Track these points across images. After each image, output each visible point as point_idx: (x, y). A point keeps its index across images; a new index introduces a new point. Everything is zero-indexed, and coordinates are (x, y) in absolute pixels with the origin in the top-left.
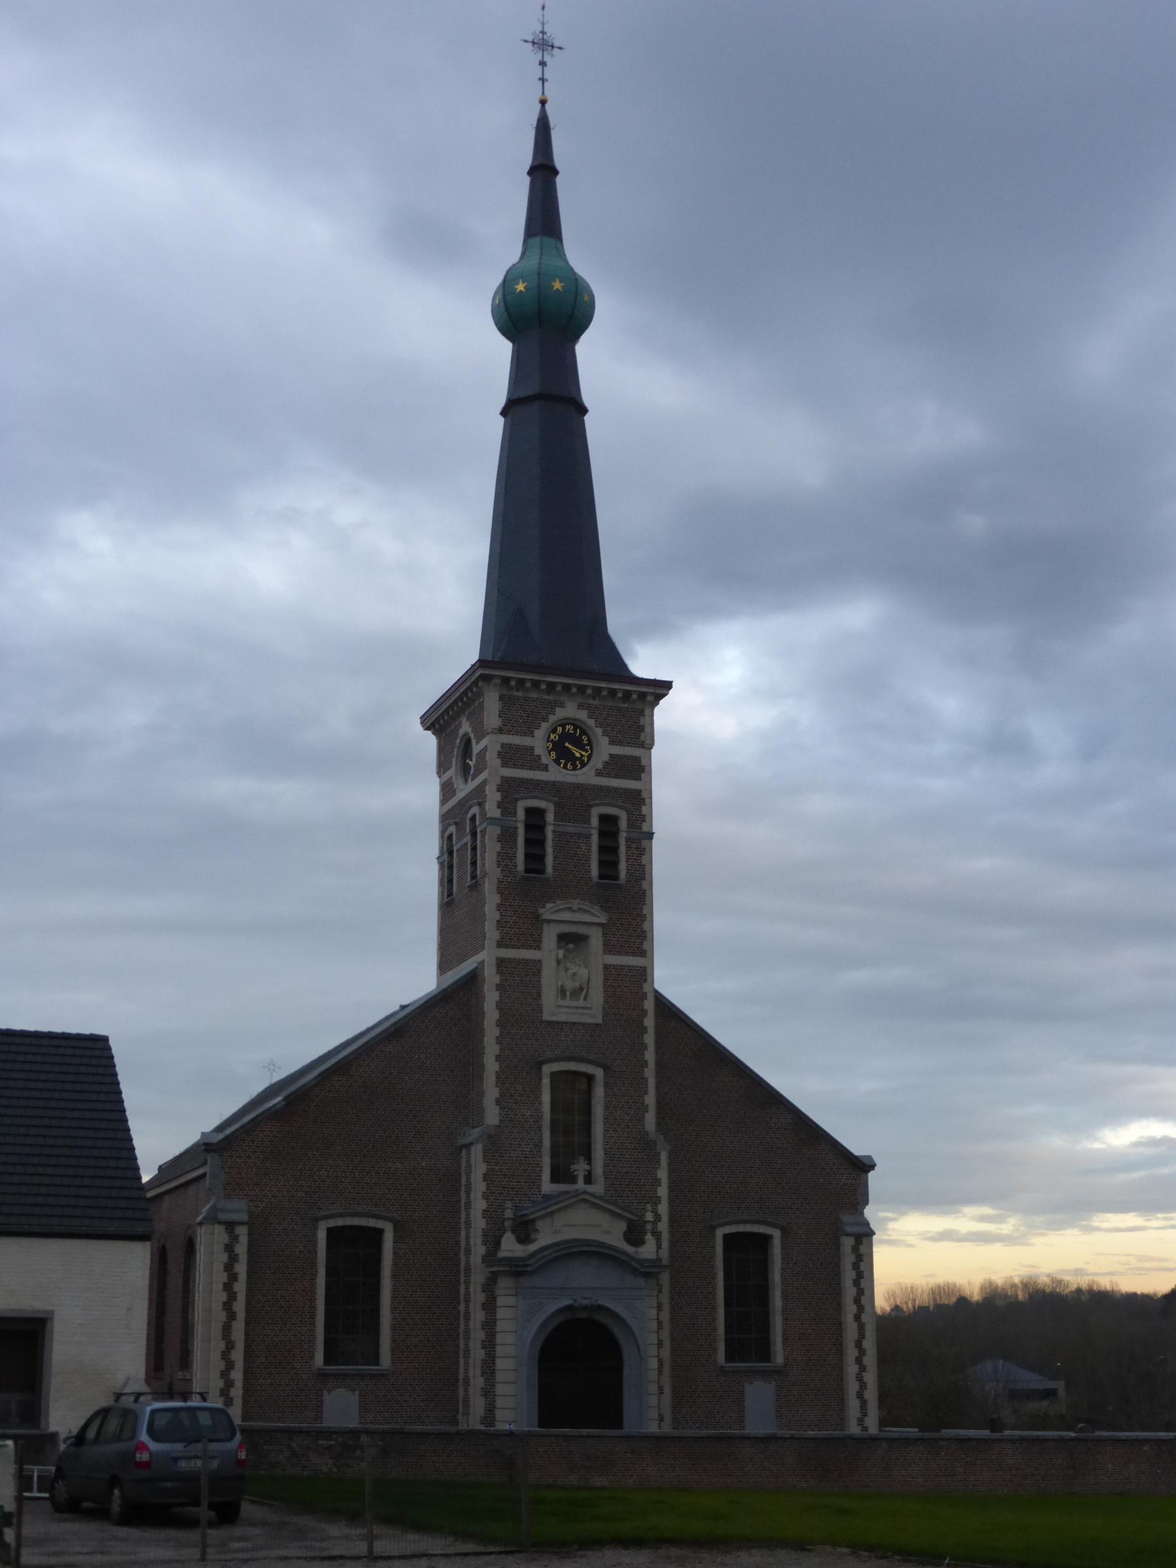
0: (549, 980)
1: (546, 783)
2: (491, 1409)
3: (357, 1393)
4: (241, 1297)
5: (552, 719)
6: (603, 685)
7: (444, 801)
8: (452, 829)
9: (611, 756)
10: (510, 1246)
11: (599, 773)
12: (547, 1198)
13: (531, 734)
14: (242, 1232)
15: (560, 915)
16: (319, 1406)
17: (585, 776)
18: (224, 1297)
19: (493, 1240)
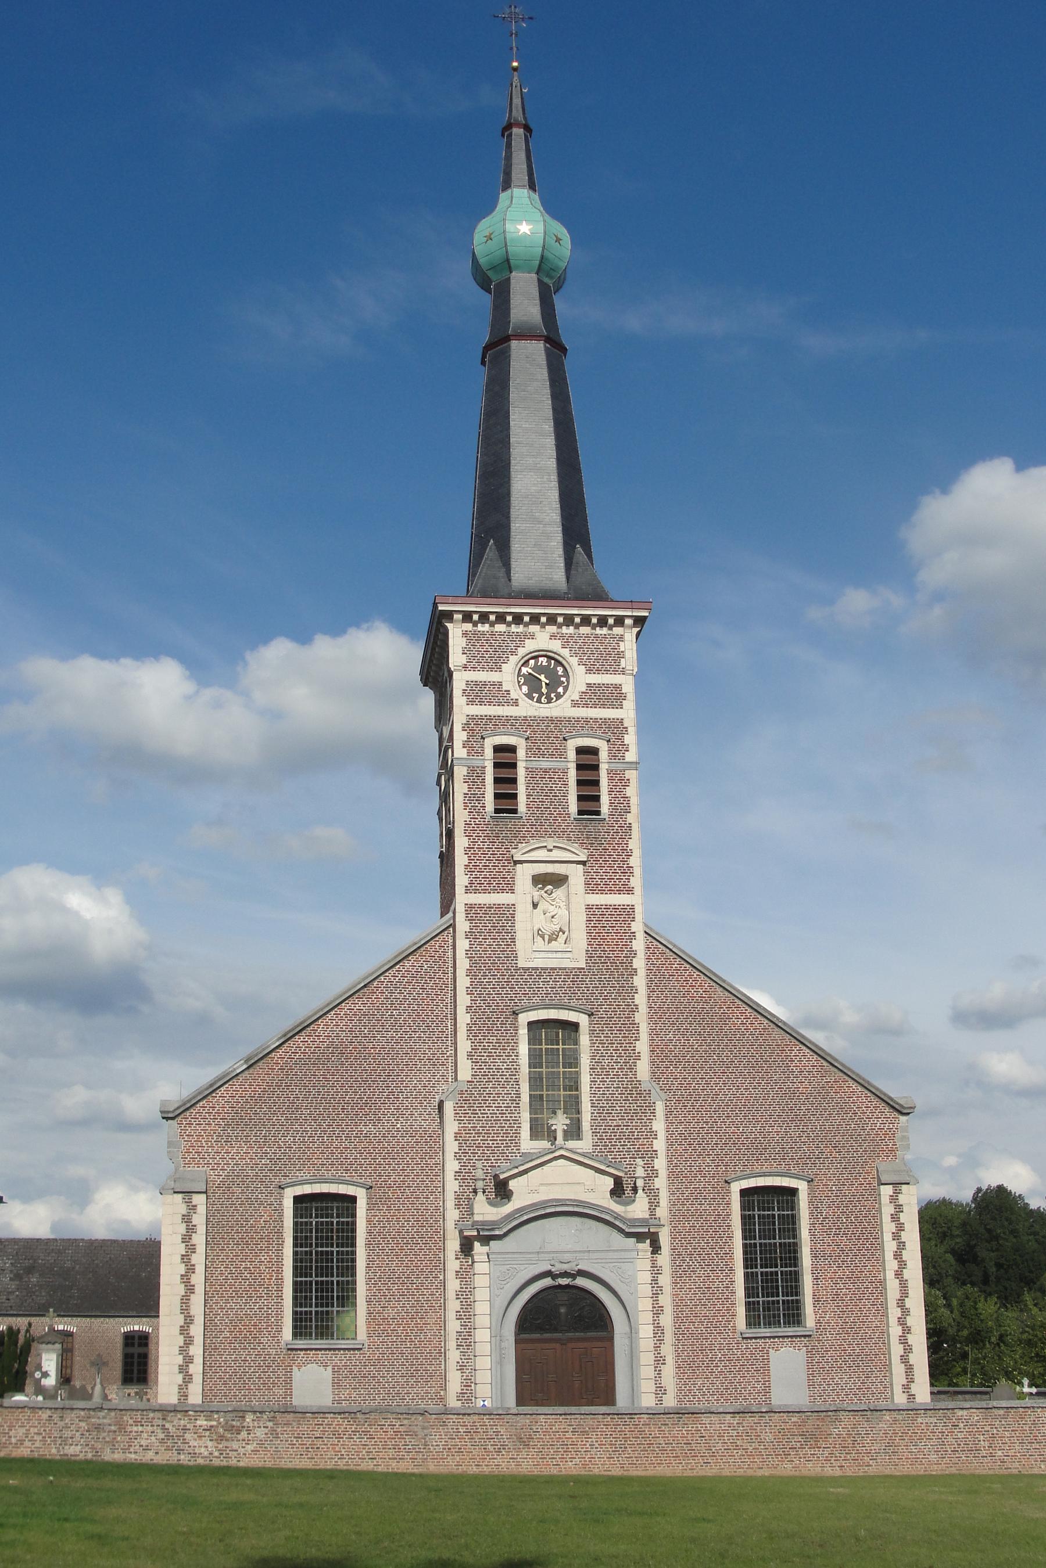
0: (526, 923)
1: (516, 719)
2: (468, 1384)
3: (330, 1369)
4: (200, 1269)
5: (521, 651)
6: (575, 611)
9: (589, 685)
10: (485, 1210)
11: (575, 704)
12: (528, 1157)
14: (199, 1200)
15: (537, 854)
16: (288, 1382)
17: (561, 708)
18: (182, 1269)
19: (465, 1205)
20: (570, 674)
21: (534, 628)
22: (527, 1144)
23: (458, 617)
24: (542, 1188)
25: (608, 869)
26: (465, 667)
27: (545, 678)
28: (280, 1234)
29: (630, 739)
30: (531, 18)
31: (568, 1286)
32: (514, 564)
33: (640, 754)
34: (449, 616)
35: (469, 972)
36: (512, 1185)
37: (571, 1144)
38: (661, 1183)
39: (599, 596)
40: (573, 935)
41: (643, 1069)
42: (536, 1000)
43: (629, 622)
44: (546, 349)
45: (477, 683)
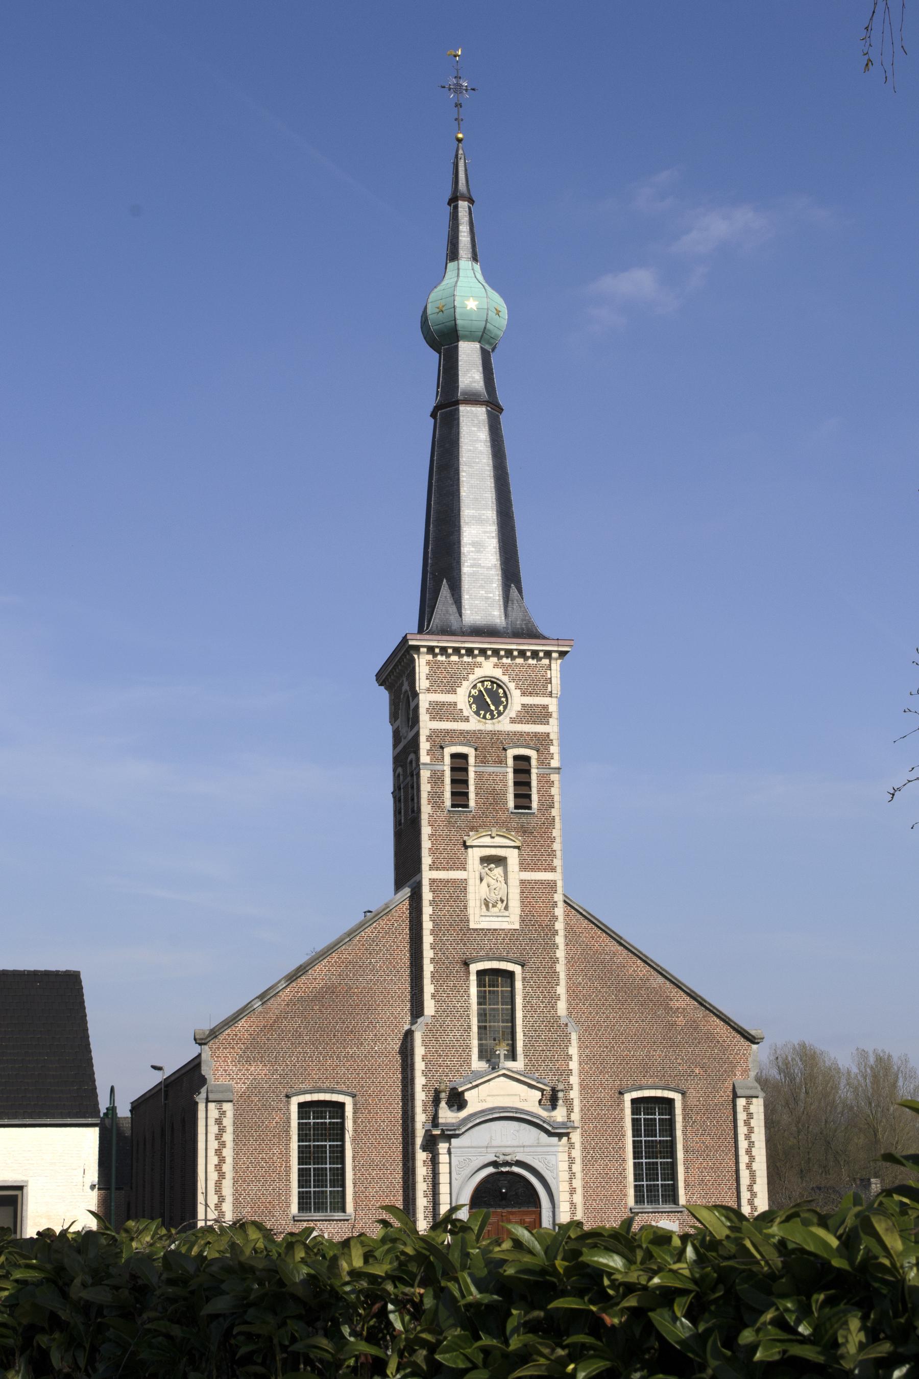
0: (476, 893)
1: (468, 732)
4: (229, 1160)
7: (395, 746)
8: (400, 770)
9: (523, 705)
11: (513, 721)
13: (455, 692)
15: (483, 843)
17: (503, 725)
20: (509, 696)
21: (480, 659)
22: (477, 1064)
23: (423, 650)
24: (489, 1099)
25: (537, 854)
26: (428, 690)
27: (489, 699)
28: (288, 1132)
29: (554, 749)
30: (473, 89)
31: (508, 1172)
32: (466, 597)
33: (562, 759)
34: (417, 648)
35: (432, 932)
36: (467, 1095)
37: (510, 1064)
38: (574, 1094)
39: (532, 634)
40: (510, 904)
41: (562, 1007)
42: (482, 953)
43: (555, 655)
44: (487, 410)
45: (437, 703)
